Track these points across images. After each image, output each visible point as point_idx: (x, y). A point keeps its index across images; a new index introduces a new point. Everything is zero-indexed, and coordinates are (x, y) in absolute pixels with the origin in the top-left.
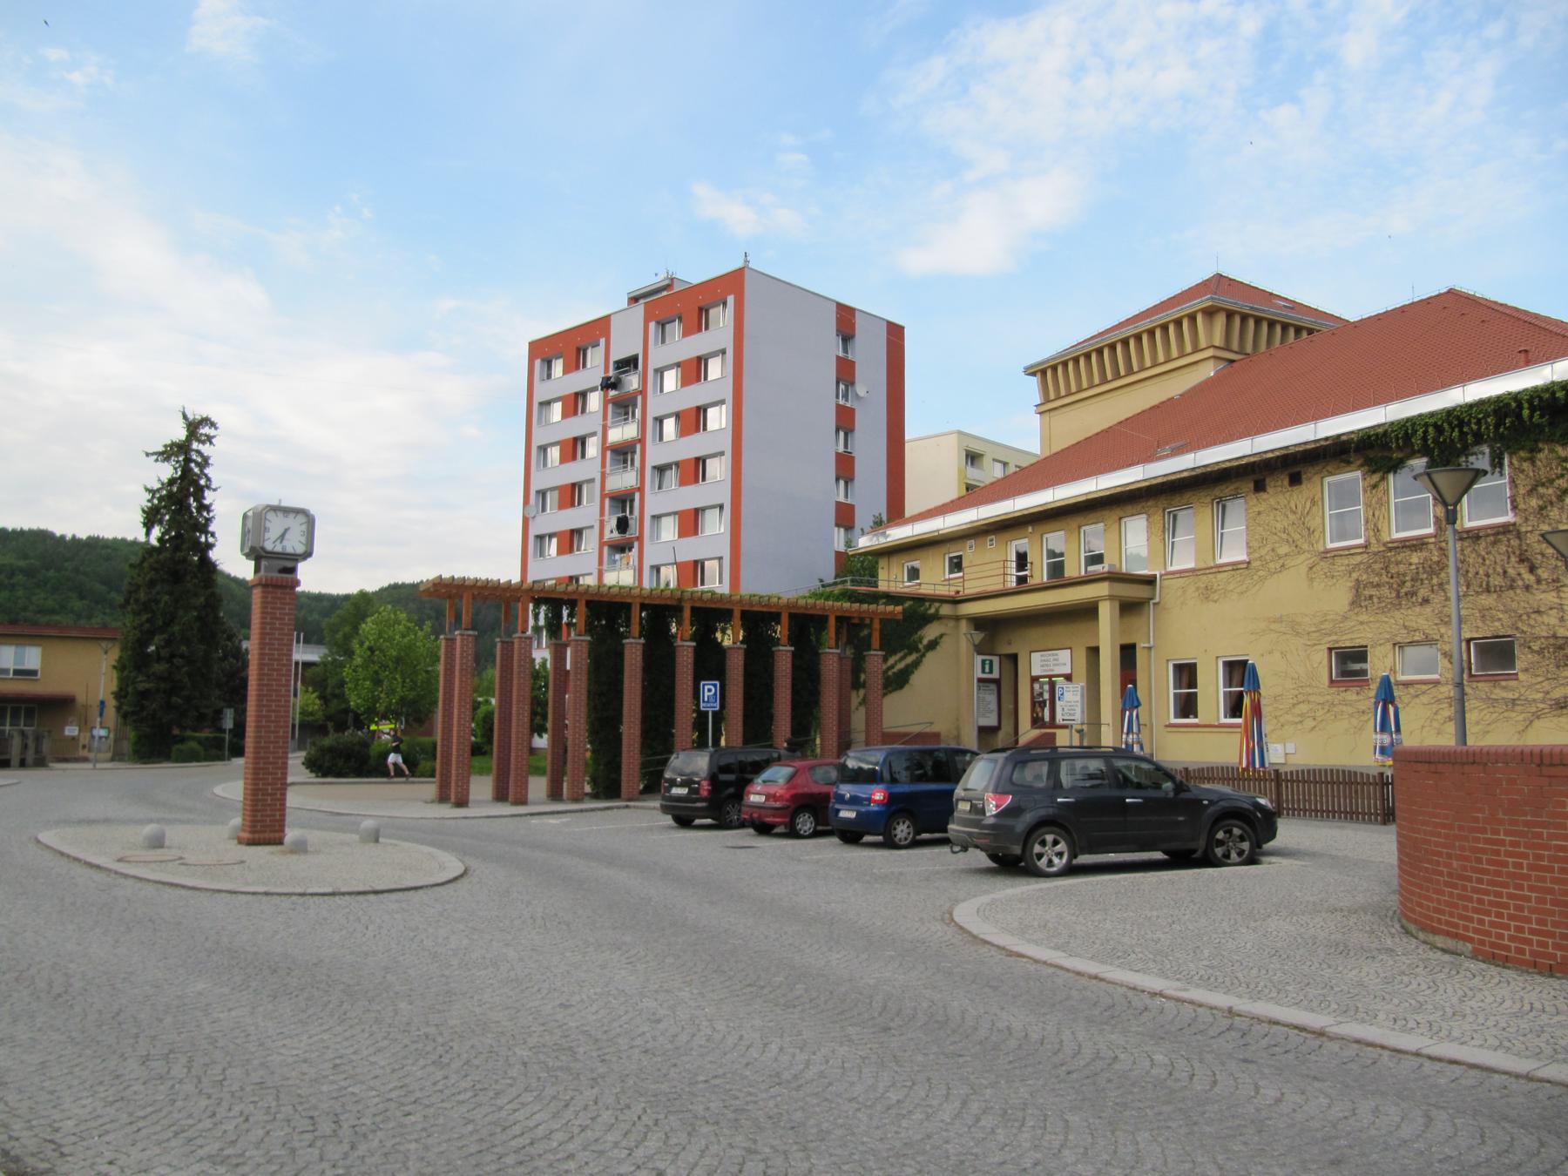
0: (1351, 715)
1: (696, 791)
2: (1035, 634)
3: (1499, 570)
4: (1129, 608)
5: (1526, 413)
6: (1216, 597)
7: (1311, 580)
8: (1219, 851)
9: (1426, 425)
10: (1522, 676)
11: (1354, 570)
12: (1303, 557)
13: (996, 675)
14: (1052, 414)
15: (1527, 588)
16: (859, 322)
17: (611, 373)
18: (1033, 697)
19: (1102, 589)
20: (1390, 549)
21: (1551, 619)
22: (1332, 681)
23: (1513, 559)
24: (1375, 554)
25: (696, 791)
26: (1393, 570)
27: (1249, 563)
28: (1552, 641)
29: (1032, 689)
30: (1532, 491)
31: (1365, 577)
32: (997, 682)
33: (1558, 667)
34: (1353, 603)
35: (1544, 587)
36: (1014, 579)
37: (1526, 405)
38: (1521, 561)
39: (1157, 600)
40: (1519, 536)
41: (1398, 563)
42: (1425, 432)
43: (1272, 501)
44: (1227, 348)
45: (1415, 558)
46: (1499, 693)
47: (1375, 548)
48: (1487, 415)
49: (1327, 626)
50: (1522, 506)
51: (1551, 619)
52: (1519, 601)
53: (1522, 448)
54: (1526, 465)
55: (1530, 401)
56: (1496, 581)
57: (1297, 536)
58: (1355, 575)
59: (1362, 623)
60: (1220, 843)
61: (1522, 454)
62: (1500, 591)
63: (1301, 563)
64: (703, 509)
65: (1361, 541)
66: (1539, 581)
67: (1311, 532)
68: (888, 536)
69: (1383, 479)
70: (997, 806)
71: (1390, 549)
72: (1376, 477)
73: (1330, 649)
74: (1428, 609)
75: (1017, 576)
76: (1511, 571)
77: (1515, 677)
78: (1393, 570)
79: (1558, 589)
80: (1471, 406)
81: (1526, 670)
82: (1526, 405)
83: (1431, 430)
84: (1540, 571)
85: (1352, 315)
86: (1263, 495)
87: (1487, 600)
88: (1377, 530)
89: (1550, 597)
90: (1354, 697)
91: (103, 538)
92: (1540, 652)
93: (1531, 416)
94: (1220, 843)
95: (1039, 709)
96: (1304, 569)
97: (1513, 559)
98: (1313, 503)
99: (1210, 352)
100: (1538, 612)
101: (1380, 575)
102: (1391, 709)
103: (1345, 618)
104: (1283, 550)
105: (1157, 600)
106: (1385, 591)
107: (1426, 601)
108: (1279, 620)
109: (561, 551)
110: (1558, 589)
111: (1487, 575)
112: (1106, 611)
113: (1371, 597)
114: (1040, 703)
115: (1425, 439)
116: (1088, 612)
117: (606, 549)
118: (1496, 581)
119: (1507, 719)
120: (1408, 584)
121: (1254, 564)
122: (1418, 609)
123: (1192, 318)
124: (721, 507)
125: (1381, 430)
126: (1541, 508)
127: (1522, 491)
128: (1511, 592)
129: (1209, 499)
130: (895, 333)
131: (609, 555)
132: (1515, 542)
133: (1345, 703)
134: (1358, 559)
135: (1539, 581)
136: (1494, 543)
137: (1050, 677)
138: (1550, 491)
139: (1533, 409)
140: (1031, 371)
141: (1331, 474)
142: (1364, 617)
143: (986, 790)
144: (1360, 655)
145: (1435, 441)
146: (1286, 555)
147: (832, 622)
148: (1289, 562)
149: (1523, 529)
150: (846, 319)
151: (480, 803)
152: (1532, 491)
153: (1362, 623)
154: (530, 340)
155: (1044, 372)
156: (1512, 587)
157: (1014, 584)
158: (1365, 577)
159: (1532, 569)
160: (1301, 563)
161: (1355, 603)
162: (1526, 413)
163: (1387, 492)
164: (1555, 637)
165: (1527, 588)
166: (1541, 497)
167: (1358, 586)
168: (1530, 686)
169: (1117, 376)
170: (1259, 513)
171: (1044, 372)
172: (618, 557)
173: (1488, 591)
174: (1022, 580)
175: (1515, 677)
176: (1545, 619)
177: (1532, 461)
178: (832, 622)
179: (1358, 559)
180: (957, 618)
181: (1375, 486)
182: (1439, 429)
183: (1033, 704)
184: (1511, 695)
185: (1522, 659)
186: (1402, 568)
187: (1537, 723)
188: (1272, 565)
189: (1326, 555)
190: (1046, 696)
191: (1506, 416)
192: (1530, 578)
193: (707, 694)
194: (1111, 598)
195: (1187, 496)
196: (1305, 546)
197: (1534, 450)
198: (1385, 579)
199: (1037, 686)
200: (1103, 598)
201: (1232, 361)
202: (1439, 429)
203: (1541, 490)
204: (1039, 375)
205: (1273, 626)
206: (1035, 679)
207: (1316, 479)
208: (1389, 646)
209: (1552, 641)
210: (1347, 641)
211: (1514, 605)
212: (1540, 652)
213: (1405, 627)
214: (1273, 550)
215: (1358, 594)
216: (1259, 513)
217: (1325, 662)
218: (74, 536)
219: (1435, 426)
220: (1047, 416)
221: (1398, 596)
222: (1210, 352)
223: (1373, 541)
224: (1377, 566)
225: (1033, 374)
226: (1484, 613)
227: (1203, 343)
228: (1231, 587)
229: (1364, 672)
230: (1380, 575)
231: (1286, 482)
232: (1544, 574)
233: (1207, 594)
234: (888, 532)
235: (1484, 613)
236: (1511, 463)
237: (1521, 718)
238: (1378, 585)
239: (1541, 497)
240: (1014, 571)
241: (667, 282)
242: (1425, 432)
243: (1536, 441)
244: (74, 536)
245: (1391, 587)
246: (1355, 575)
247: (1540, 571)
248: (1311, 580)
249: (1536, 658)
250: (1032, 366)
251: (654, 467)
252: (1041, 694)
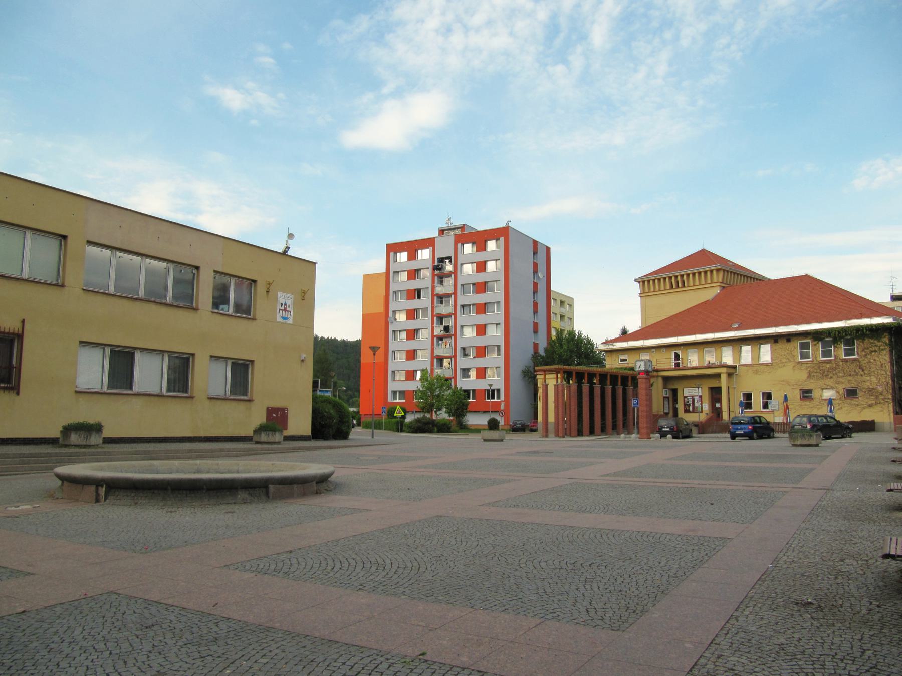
0: (807, 408)
1: (673, 429)
2: (685, 382)
3: (853, 370)
4: (730, 375)
5: (865, 331)
6: (760, 373)
7: (794, 370)
8: (845, 435)
9: (836, 331)
10: (860, 398)
11: (808, 368)
12: (790, 363)
13: (668, 395)
14: (647, 297)
15: (862, 375)
16: (539, 247)
17: (436, 264)
18: (684, 403)
19: (724, 370)
20: (820, 363)
21: (868, 383)
22: (801, 399)
23: (857, 367)
24: (815, 363)
25: (673, 429)
26: (821, 368)
27: (772, 364)
28: (868, 389)
29: (684, 400)
30: (863, 350)
31: (812, 370)
32: (668, 398)
33: (870, 396)
34: (808, 377)
35: (866, 375)
36: (674, 364)
37: (865, 329)
38: (860, 368)
39: (737, 373)
40: (859, 361)
41: (823, 366)
42: (835, 333)
43: (780, 346)
44: (722, 283)
45: (828, 365)
46: (853, 402)
47: (815, 362)
48: (854, 330)
49: (800, 383)
50: (860, 354)
51: (868, 383)
52: (859, 378)
53: (861, 339)
54: (861, 343)
55: (866, 328)
56: (853, 373)
57: (789, 357)
58: (809, 369)
59: (811, 383)
60: (845, 434)
61: (861, 340)
62: (853, 375)
63: (791, 364)
64: (487, 325)
65: (811, 359)
66: (865, 374)
67: (794, 356)
68: (615, 345)
69: (818, 343)
70: (810, 425)
71: (820, 363)
72: (816, 342)
73: (800, 390)
74: (832, 380)
75: (675, 363)
76: (857, 371)
77: (858, 398)
78: (821, 368)
79: (870, 376)
80: (849, 327)
81: (861, 396)
82: (865, 329)
83: (837, 332)
84: (865, 371)
85: (773, 278)
86: (777, 344)
87: (849, 378)
88: (816, 357)
89: (868, 378)
90: (809, 403)
91: (322, 338)
92: (865, 392)
93: (866, 332)
94: (845, 434)
95: (687, 407)
96: (792, 366)
97: (857, 367)
98: (795, 348)
99: (718, 284)
100: (865, 382)
101: (817, 370)
102: (833, 407)
103: (805, 381)
104: (784, 360)
105: (737, 373)
106: (819, 374)
107: (831, 377)
108: (783, 381)
109: (408, 338)
110: (870, 376)
111: (850, 371)
112: (724, 377)
113: (814, 375)
114: (687, 405)
115: (835, 335)
116: (718, 376)
117: (435, 339)
118: (853, 373)
119: (856, 409)
120: (826, 372)
121: (774, 364)
122: (829, 379)
123: (711, 271)
124: (498, 324)
125: (821, 331)
126: (866, 355)
127: (860, 350)
128: (857, 376)
129: (756, 344)
130: (548, 250)
131: (437, 341)
132: (858, 363)
133: (806, 405)
134: (810, 364)
135: (865, 374)
136: (852, 363)
137: (692, 396)
138: (868, 350)
139: (867, 330)
140: (636, 280)
141: (800, 340)
142: (812, 381)
143: (807, 423)
144: (810, 391)
145: (838, 335)
146: (786, 362)
147: (609, 376)
148: (786, 364)
149: (860, 360)
150: (535, 243)
151: (551, 437)
152: (863, 350)
153: (811, 383)
154: (387, 243)
155: (644, 282)
156: (857, 375)
157: (674, 366)
158: (812, 370)
159: (863, 370)
160: (791, 364)
161: (809, 377)
162: (865, 331)
163: (819, 347)
164: (869, 388)
165: (862, 375)
166: (866, 352)
167: (810, 372)
168: (862, 401)
169: (678, 287)
170: (776, 349)
171: (644, 282)
172: (440, 342)
173: (850, 375)
174: (677, 365)
175: (858, 398)
176: (867, 383)
177: (863, 343)
178: (609, 376)
179: (810, 364)
180: (658, 376)
181: (815, 345)
182: (839, 333)
183: (685, 405)
184: (857, 403)
185: (860, 394)
186: (824, 368)
187: (864, 410)
188: (780, 365)
189: (799, 363)
190: (691, 402)
191: (859, 331)
192: (862, 373)
193: (634, 402)
194: (726, 372)
195: (748, 341)
196: (792, 360)
197: (864, 339)
198: (818, 370)
199: (686, 399)
200: (723, 373)
201: (724, 287)
202: (839, 333)
203: (866, 350)
204: (641, 283)
205: (781, 382)
206: (686, 397)
207: (796, 341)
208: (820, 389)
209: (868, 389)
210: (806, 387)
211: (858, 379)
212: (865, 392)
213: (825, 384)
214: (781, 360)
215: (810, 375)
216: (776, 349)
217: (799, 393)
218: (335, 338)
219: (838, 331)
220: (644, 298)
221: (823, 376)
222: (718, 284)
223: (815, 360)
224: (816, 367)
225: (639, 282)
226: (849, 381)
227: (715, 280)
228: (765, 370)
229: (811, 396)
230: (817, 370)
231: (785, 341)
232: (866, 372)
233: (756, 372)
234: (614, 344)
235: (849, 381)
236: (857, 343)
237: (859, 409)
238: (816, 372)
239: (866, 352)
240: (674, 361)
241: (462, 226)
242: (835, 333)
243: (864, 337)
244: (335, 338)
245: (820, 373)
246: (809, 369)
247: (865, 371)
248: (794, 370)
249: (864, 393)
250: (638, 279)
251: (461, 306)
252: (688, 402)
